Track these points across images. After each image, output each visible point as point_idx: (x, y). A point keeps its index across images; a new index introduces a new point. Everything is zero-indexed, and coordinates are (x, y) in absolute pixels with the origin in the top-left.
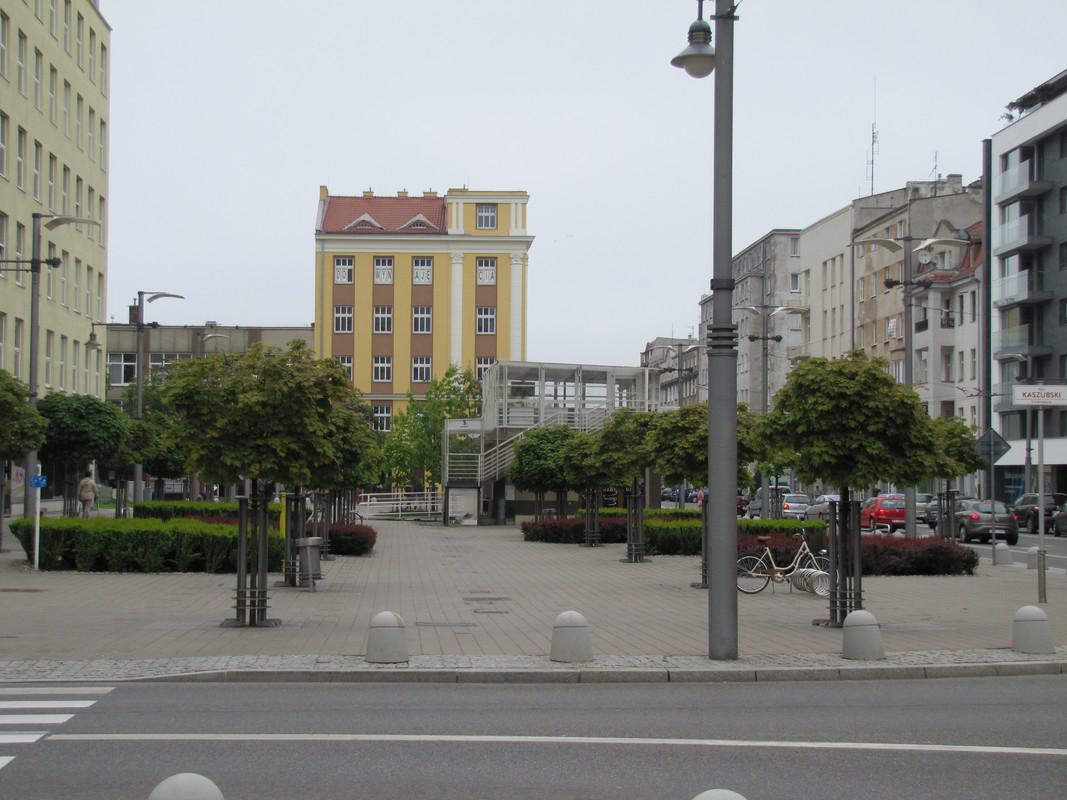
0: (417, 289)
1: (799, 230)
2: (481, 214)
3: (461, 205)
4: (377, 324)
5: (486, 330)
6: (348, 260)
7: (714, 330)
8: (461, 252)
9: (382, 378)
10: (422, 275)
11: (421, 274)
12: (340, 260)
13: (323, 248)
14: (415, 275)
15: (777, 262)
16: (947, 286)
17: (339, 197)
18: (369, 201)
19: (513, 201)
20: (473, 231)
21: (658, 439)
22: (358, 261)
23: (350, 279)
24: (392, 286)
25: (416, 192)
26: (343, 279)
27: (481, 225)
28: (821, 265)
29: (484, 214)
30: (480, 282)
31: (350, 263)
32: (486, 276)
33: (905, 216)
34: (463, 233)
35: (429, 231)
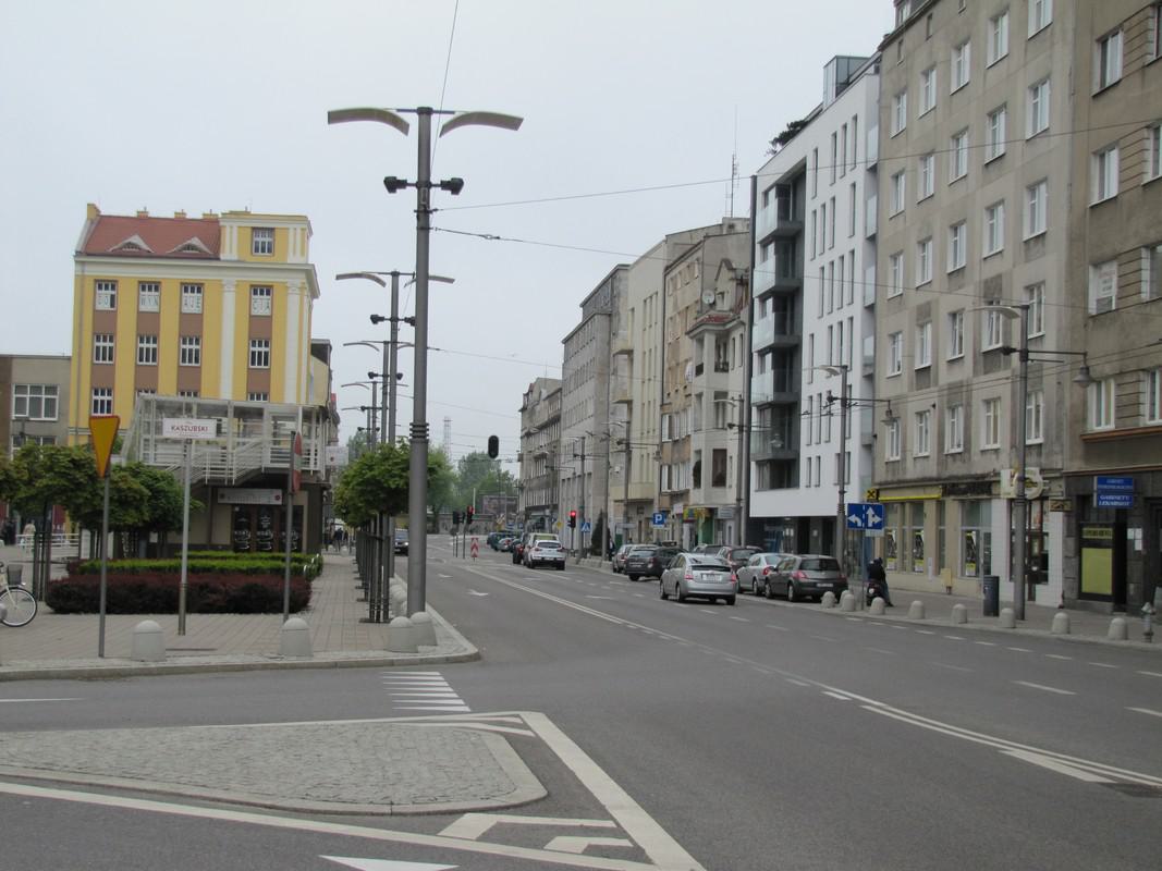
0: (142, 317)
1: (628, 266)
2: (257, 239)
3: (235, 229)
4: (266, 358)
5: (104, 359)
6: (111, 284)
9: (102, 411)
10: (192, 303)
11: (190, 301)
12: (101, 284)
13: (83, 271)
14: (183, 303)
15: (622, 300)
16: (721, 328)
17: (110, 217)
18: (143, 222)
19: (291, 227)
22: (120, 286)
23: (112, 305)
24: (269, 318)
25: (195, 213)
26: (104, 305)
27: (257, 250)
28: (642, 303)
29: (260, 239)
30: (254, 312)
31: (113, 288)
32: (261, 306)
33: (699, 254)
35: (203, 257)
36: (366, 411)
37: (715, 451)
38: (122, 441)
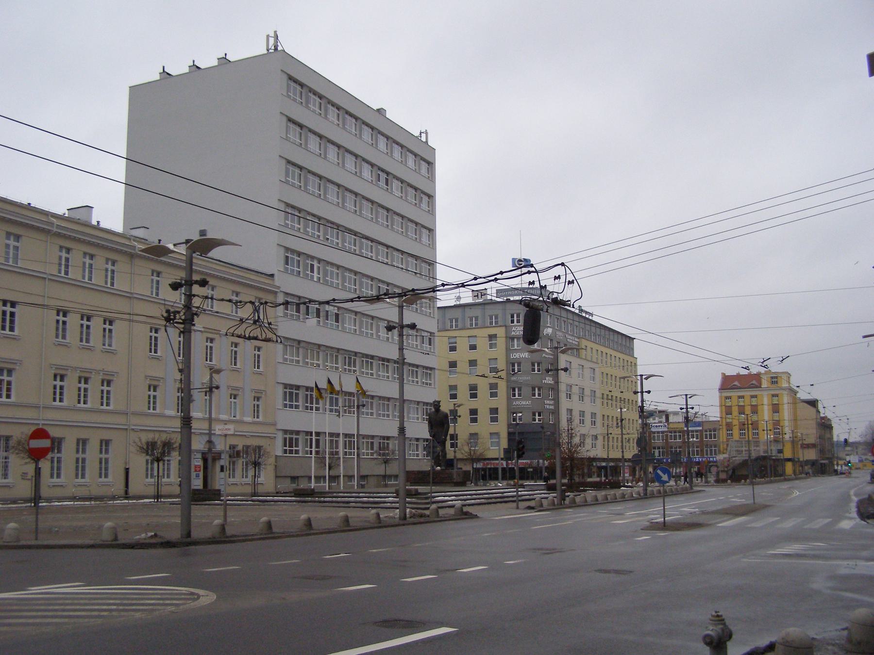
7: (184, 418)
8: (766, 393)
12: (727, 398)
20: (770, 386)
21: (337, 411)
29: (773, 380)
34: (766, 386)
35: (756, 387)
36: (396, 331)
37: (497, 409)
38: (390, 463)
